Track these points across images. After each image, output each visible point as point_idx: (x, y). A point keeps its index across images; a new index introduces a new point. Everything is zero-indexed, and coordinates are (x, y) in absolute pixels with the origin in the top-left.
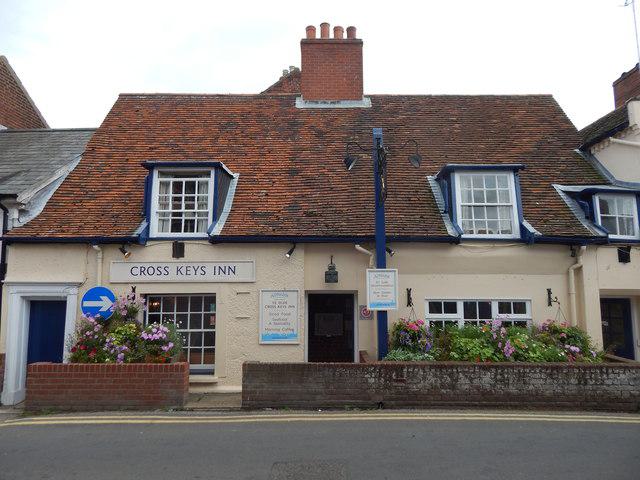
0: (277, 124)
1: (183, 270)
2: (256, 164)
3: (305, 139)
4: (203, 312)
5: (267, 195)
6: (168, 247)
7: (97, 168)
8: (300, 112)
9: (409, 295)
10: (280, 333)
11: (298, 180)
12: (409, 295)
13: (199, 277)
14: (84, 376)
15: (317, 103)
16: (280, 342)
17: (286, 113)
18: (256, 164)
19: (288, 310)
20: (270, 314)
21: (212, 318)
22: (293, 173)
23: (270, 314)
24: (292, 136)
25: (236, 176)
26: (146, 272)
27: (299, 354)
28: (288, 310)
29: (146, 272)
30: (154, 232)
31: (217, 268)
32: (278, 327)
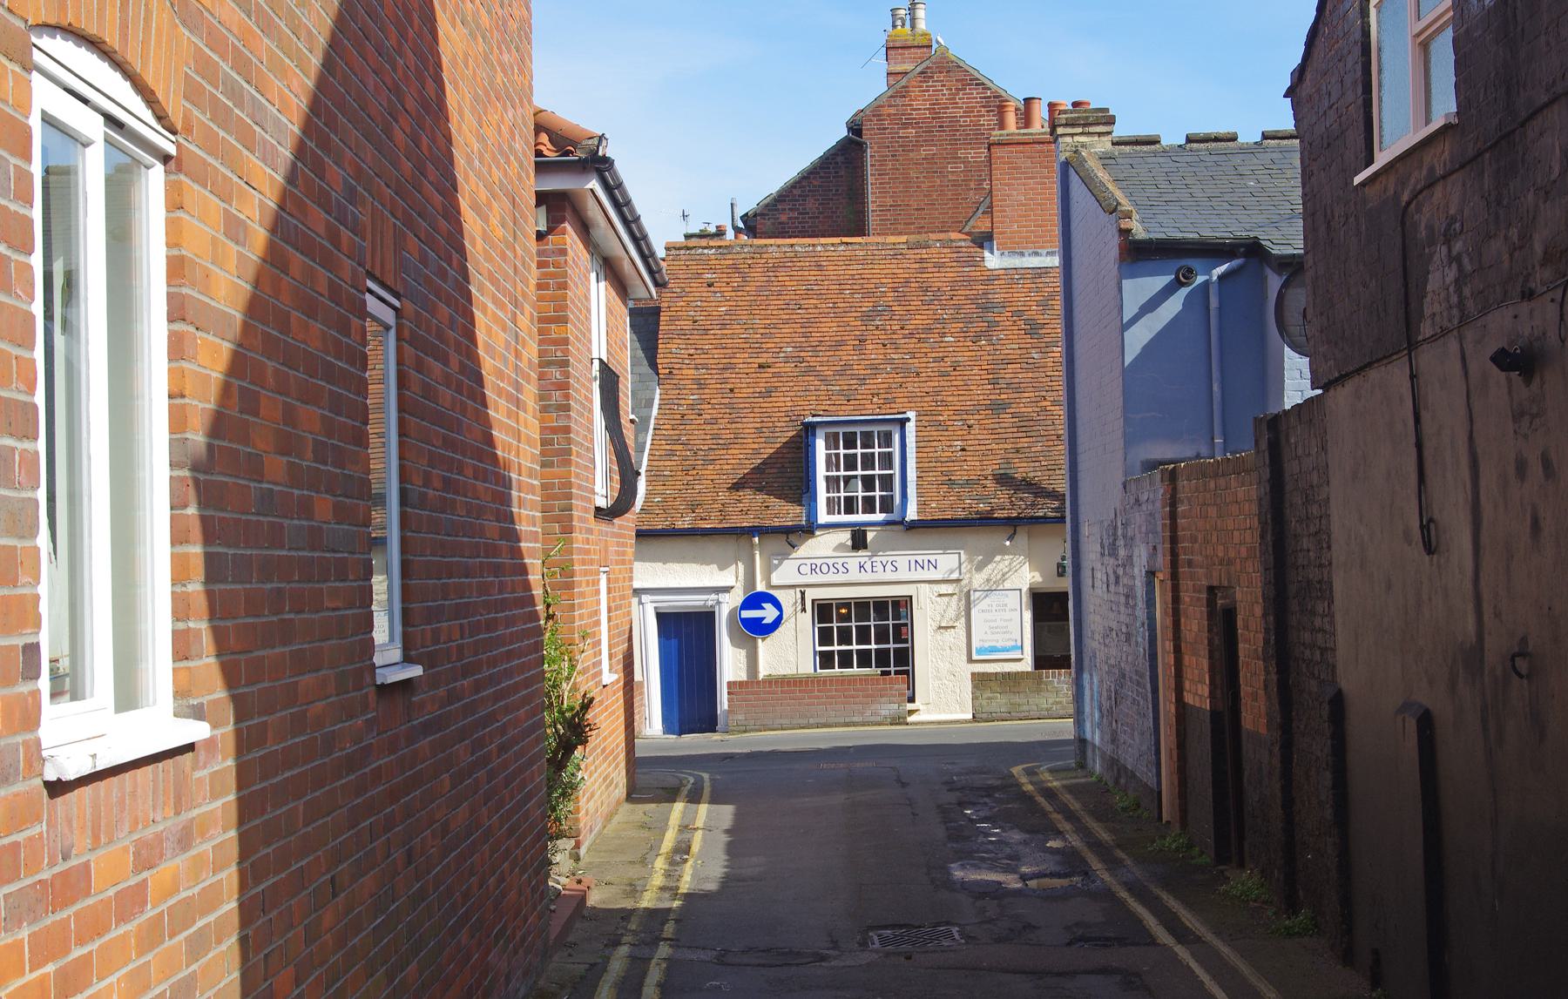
0: (958, 308)
1: (868, 566)
2: (938, 393)
3: (1010, 342)
4: (891, 622)
5: (963, 450)
6: (845, 537)
7: (691, 406)
8: (992, 277)
9: (72, 137)
10: (999, 645)
11: (1007, 419)
12: (72, 137)
13: (889, 576)
14: (793, 692)
15: (1022, 254)
16: (1214, 370)
17: (970, 281)
18: (938, 393)
19: (1007, 615)
20: (986, 621)
21: (904, 629)
22: (997, 408)
23: (986, 621)
24: (986, 333)
25: (911, 415)
26: (818, 570)
27: (1027, 665)
28: (1007, 615)
29: (818, 570)
30: (823, 517)
31: (926, 562)
32: (996, 637)
